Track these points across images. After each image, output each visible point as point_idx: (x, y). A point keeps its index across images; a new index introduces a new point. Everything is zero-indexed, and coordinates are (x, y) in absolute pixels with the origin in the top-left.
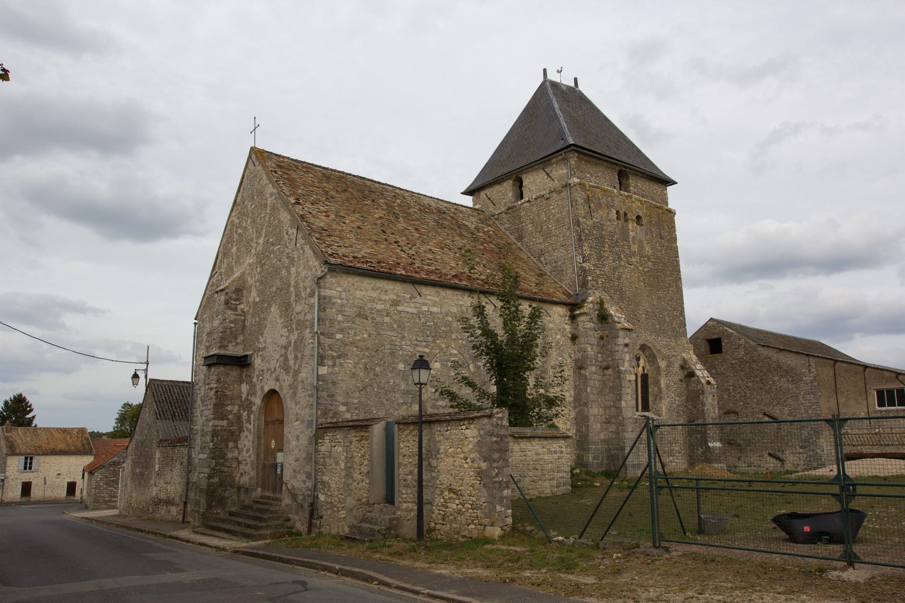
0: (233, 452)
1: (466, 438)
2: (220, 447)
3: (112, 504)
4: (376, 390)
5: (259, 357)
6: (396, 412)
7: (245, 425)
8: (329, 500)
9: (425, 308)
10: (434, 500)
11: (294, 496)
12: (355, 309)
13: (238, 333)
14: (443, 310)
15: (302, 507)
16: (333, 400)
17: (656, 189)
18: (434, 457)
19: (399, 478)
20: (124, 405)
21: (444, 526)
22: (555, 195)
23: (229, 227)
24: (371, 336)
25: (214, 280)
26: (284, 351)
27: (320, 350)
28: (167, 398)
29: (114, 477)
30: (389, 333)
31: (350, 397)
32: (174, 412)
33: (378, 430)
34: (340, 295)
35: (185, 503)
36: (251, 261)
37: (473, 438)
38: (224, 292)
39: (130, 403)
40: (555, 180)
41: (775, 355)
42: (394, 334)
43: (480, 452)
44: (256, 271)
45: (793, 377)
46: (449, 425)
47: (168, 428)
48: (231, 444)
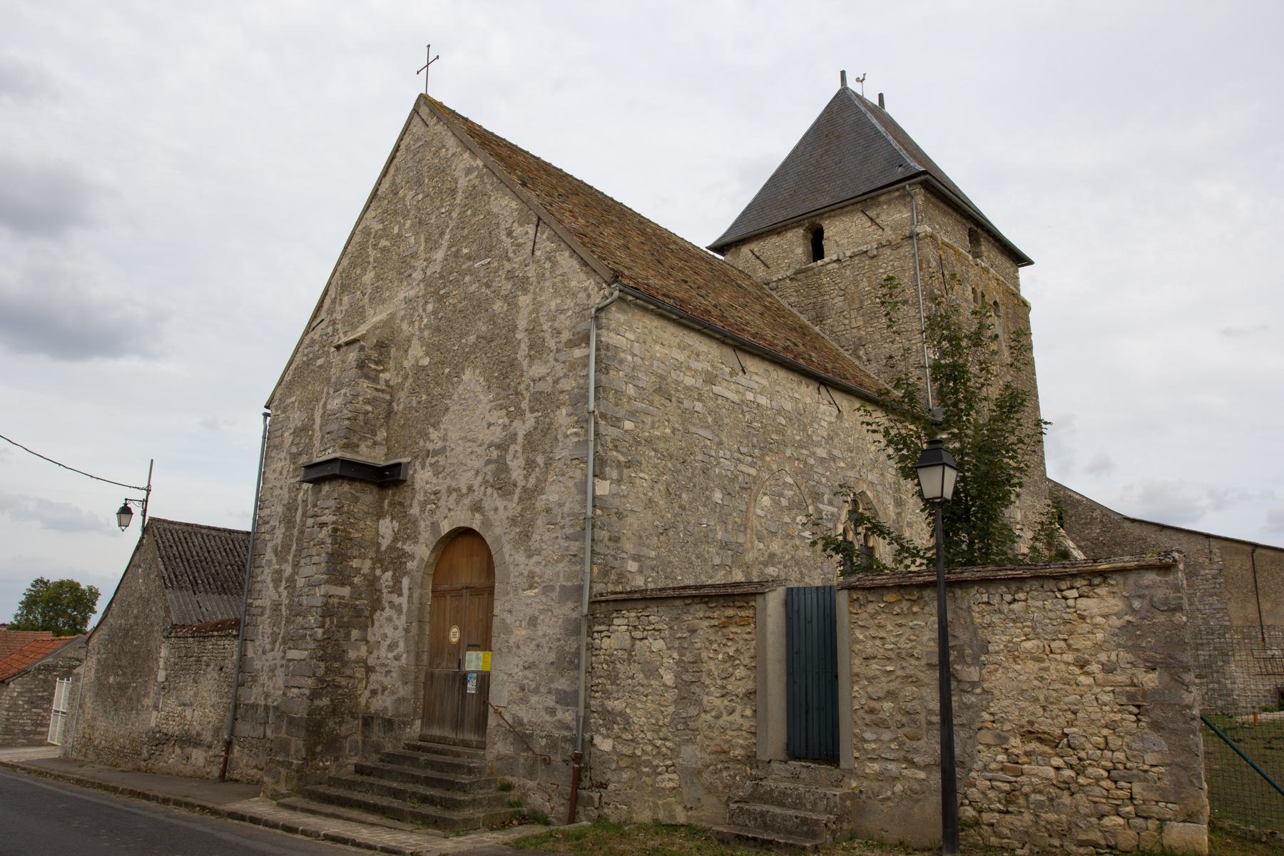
0: (358, 649)
2: (335, 637)
3: (37, 737)
4: (682, 535)
5: (428, 468)
7: (386, 597)
8: (627, 750)
9: (750, 396)
10: (972, 757)
13: (378, 423)
14: (774, 403)
15: (547, 762)
16: (618, 548)
18: (969, 660)
20: (37, 581)
22: (888, 251)
23: (357, 239)
24: (677, 432)
25: (316, 335)
26: (495, 454)
27: (599, 448)
28: (182, 553)
29: (44, 691)
30: (701, 432)
31: (644, 545)
32: (194, 578)
34: (632, 346)
35: (229, 745)
36: (412, 293)
37: (1105, 616)
38: (357, 346)
39: (46, 580)
40: (887, 229)
41: (1153, 536)
44: (424, 310)
46: (1020, 589)
47: (186, 605)
48: (355, 633)
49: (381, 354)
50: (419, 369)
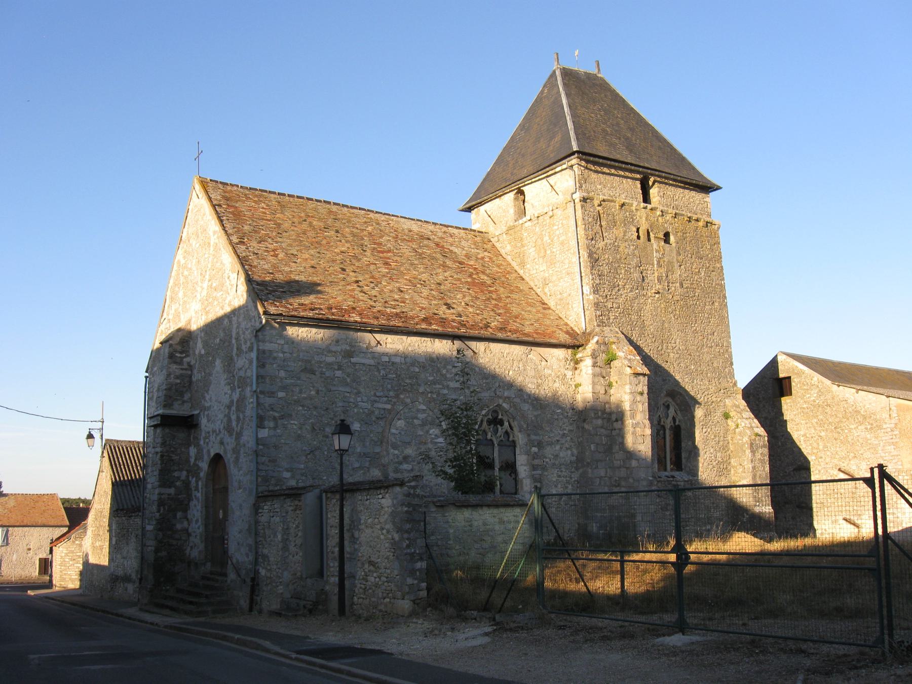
1: (382, 507)
4: (326, 453)
6: (351, 478)
7: (195, 493)
8: (268, 575)
11: (237, 571)
12: (300, 363)
17: (693, 197)
19: (327, 550)
21: (364, 600)
24: (320, 393)
33: (310, 498)
37: (388, 507)
42: (348, 390)
43: (394, 523)
45: (872, 424)
48: (179, 514)
49: (183, 347)
50: (201, 356)
